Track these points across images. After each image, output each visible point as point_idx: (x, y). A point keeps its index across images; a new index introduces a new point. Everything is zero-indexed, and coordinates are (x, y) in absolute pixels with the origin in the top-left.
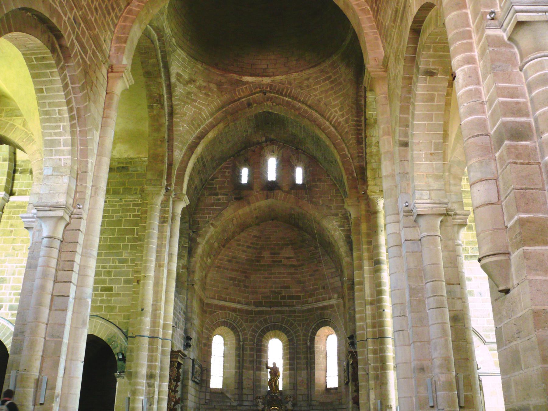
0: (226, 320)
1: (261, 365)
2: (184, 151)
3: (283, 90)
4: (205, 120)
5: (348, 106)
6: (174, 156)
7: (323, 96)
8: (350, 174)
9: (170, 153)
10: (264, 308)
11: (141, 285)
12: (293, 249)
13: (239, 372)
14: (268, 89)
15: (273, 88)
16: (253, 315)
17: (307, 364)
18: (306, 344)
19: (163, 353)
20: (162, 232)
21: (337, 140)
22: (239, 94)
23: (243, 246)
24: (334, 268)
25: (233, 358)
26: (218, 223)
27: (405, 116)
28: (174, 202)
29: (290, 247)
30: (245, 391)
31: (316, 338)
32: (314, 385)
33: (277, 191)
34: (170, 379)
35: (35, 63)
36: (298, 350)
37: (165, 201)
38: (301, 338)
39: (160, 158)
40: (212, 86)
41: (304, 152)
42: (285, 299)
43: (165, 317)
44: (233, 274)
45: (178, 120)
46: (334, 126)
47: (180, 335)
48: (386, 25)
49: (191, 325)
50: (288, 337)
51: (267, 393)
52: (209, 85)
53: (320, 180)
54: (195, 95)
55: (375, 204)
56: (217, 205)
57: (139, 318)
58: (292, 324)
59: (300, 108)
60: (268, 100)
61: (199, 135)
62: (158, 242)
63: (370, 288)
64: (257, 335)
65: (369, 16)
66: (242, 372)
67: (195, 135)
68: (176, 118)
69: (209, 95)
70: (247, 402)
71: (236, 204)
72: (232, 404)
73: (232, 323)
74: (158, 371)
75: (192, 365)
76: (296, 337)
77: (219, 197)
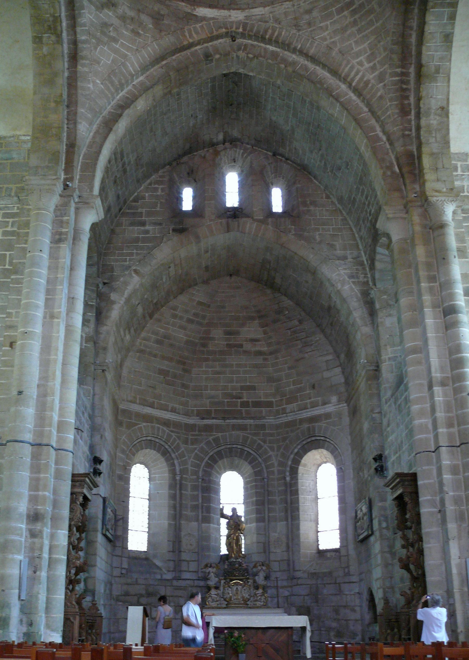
0: (153, 439)
1: (210, 513)
2: (95, 127)
3: (266, 31)
4: (132, 76)
5: (385, 50)
6: (78, 132)
8: (388, 168)
9: (71, 126)
10: (214, 421)
11: (17, 352)
13: (176, 524)
14: (241, 30)
15: (248, 28)
16: (197, 433)
17: (286, 511)
18: (284, 478)
19: (58, 475)
20: (57, 258)
21: (361, 114)
22: (191, 36)
23: (181, 318)
24: (331, 354)
25: (164, 502)
26: (146, 270)
28: (77, 209)
29: (256, 321)
30: (184, 556)
31: (301, 469)
32: (298, 545)
33: (244, 219)
34: (70, 526)
36: (270, 489)
37: (61, 205)
38: (275, 469)
39: (54, 131)
40: (144, 18)
41: (287, 159)
42: (249, 407)
43: (61, 409)
44: (165, 365)
45: (86, 69)
47: (84, 453)
49: (101, 437)
50: (253, 467)
51: (219, 560)
52: (139, 16)
53: (313, 203)
54: (116, 29)
55: (442, 213)
56: (144, 240)
57: (13, 409)
59: (294, 63)
60: (239, 49)
61: (121, 103)
62: (48, 274)
63: (439, 357)
64: (203, 464)
66: (180, 524)
67: (115, 101)
68: (83, 65)
69: (138, 34)
70: (188, 573)
71: (175, 238)
72: (165, 577)
73: (163, 443)
74: (49, 508)
75: (101, 508)
76: (267, 467)
77: (147, 227)
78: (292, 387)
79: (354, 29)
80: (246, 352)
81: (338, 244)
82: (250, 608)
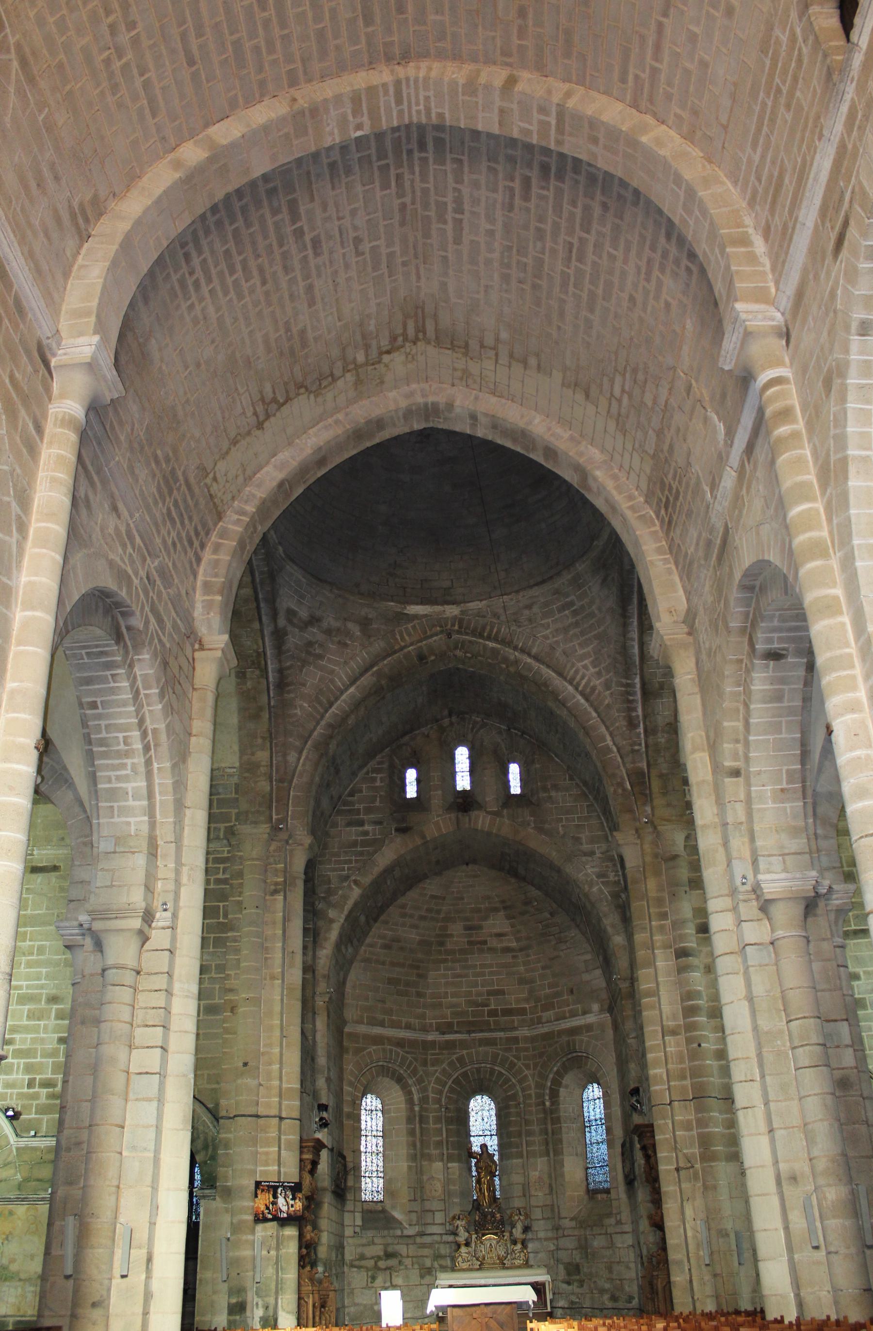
3: (484, 628)
5: (609, 656)
7: (560, 637)
12: (508, 917)
14: (456, 627)
17: (547, 1144)
18: (544, 1104)
22: (403, 639)
23: (412, 916)
27: (733, 724)
29: (502, 913)
33: (476, 812)
35: (86, 661)
38: (532, 1092)
42: (497, 1016)
45: (292, 695)
46: (582, 694)
48: (686, 553)
53: (555, 787)
54: (321, 646)
58: (512, 1065)
59: (517, 662)
60: (456, 648)
65: (653, 529)
66: (421, 1166)
69: (346, 645)
72: (406, 1233)
76: (523, 1090)
77: (367, 827)
78: (547, 991)
79: (577, 630)
80: (492, 950)
81: (584, 836)
82: (507, 1268)
